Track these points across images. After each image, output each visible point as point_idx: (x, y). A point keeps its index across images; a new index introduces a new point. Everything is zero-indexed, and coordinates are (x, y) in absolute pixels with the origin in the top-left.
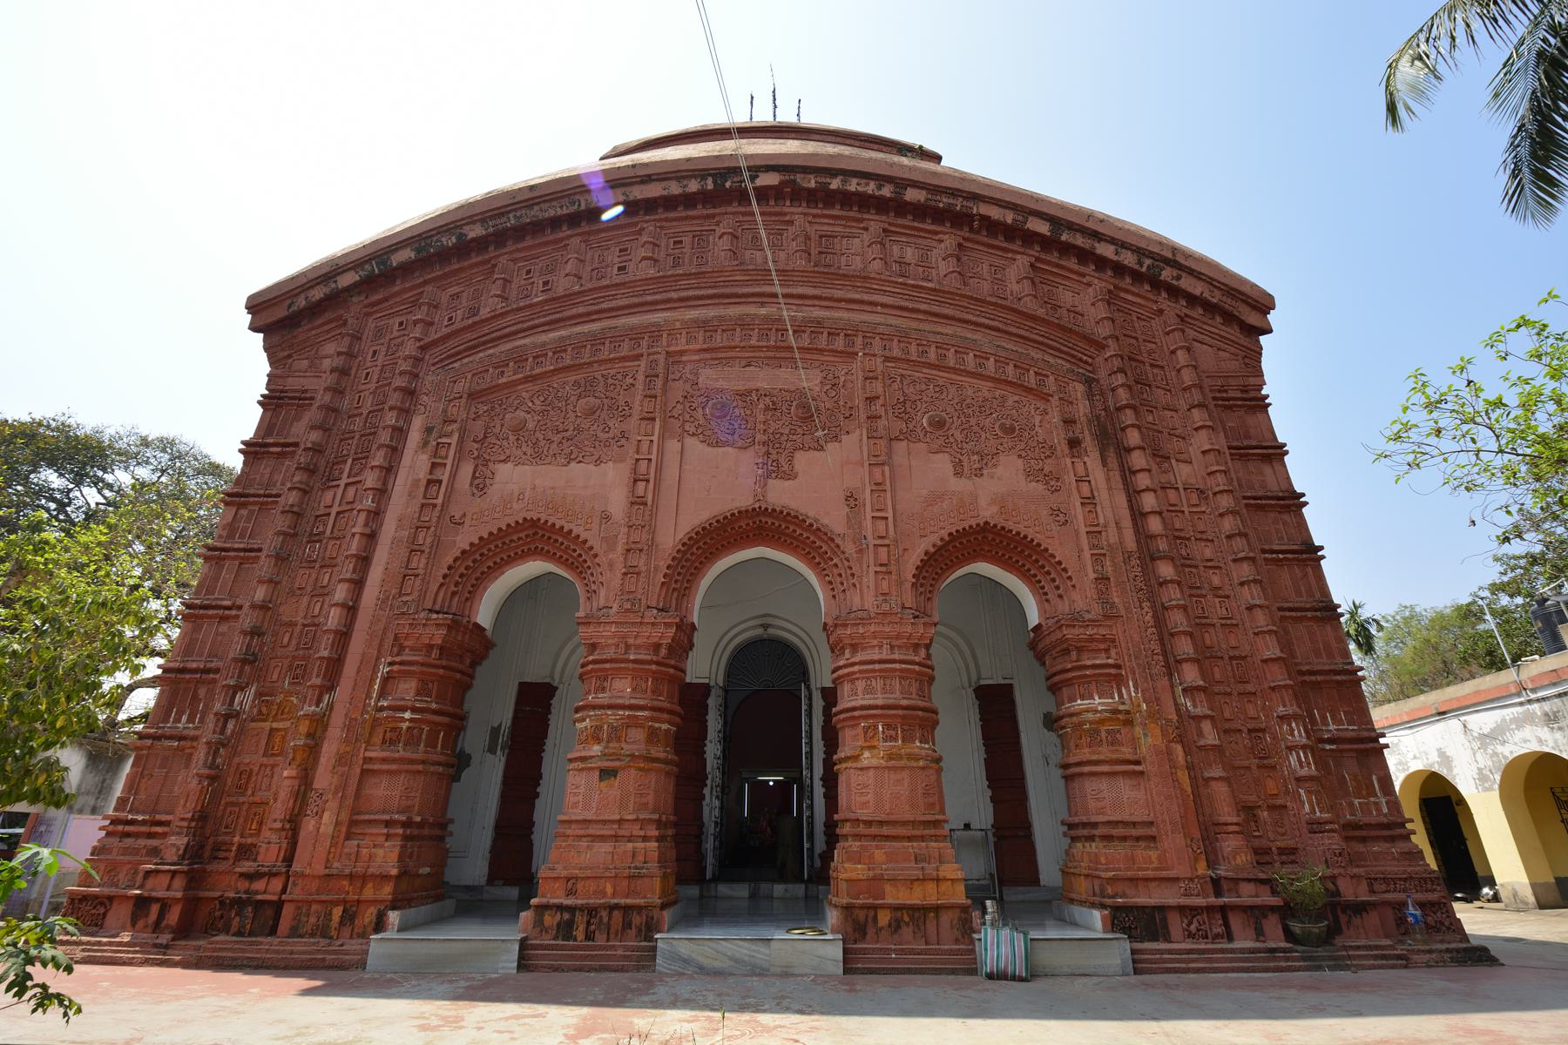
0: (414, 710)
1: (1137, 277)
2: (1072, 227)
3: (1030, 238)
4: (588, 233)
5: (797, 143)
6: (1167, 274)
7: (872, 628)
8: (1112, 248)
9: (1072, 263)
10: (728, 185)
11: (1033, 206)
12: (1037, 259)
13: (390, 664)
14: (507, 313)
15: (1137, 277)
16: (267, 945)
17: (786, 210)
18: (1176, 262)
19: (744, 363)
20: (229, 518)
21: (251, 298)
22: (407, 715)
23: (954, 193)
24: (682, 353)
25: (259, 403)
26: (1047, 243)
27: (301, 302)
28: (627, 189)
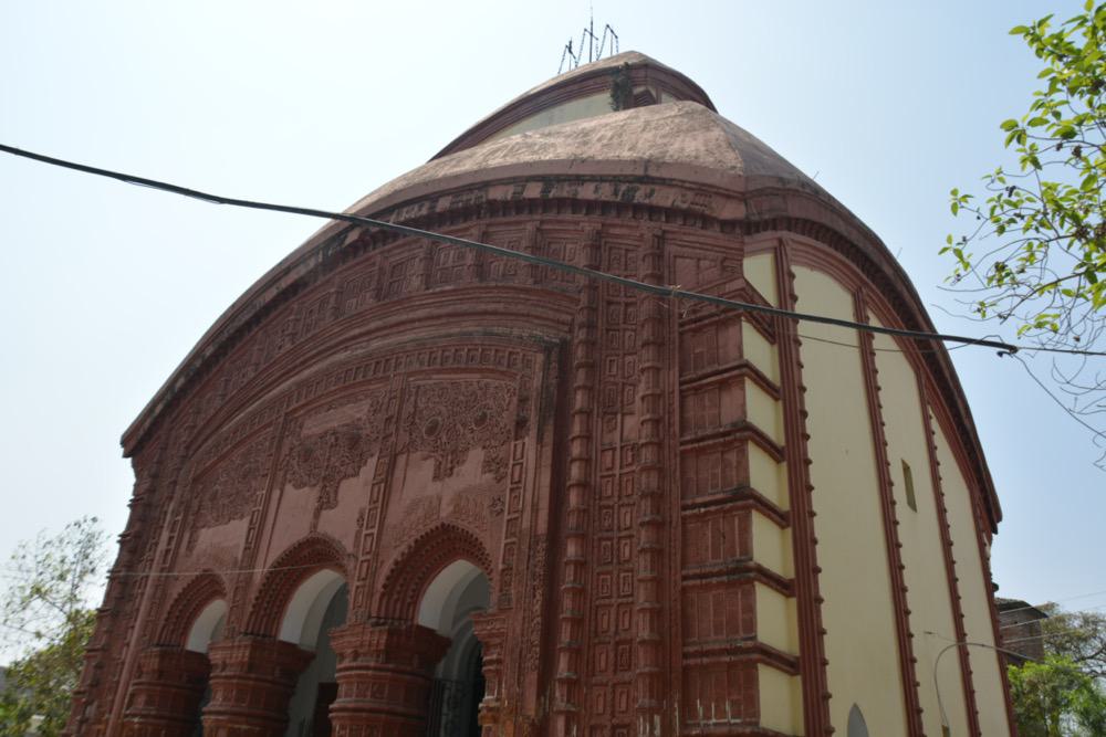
0: (143, 716)
1: (620, 208)
2: (560, 179)
3: (531, 205)
4: (266, 325)
5: (268, 300)
6: (639, 197)
7: (346, 639)
8: (592, 186)
9: (568, 216)
10: (330, 252)
11: (527, 173)
12: (542, 222)
13: (136, 684)
14: (196, 438)
15: (620, 208)
16: (784, 591)
17: (370, 254)
18: (647, 177)
19: (326, 407)
20: (613, 189)
21: (125, 441)
22: (136, 720)
23: (470, 188)
24: (295, 410)
25: (129, 506)
26: (544, 204)
27: (141, 432)
28: (278, 284)
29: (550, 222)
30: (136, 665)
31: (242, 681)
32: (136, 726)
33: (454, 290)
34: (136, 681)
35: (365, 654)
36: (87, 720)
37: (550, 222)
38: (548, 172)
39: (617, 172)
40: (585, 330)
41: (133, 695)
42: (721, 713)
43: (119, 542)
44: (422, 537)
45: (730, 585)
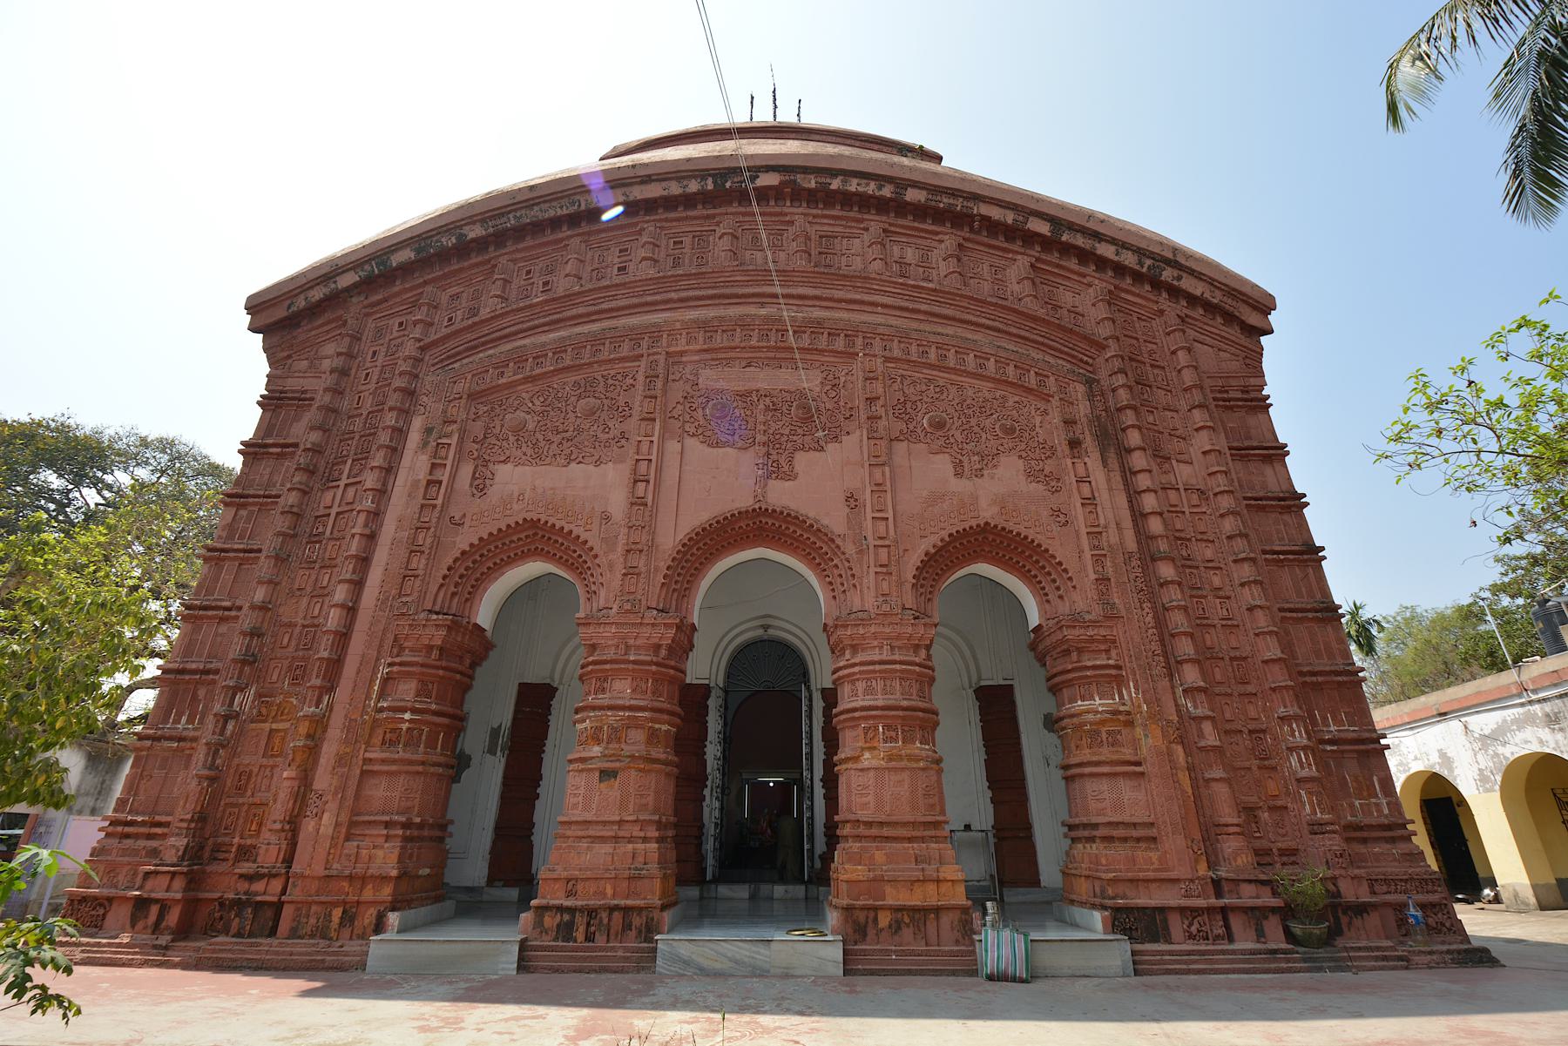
0: (414, 711)
2: (1072, 227)
3: (1030, 238)
10: (728, 185)
11: (1033, 206)
13: (390, 665)
15: (1138, 277)
17: (786, 210)
22: (407, 716)
23: (954, 193)
29: (1044, 262)
30: (390, 637)
31: (448, 674)
32: (405, 726)
33: (935, 290)
34: (389, 660)
35: (412, 650)
36: (237, 715)
37: (1044, 262)
38: (1060, 214)
39: (1143, 245)
40: (335, 376)
41: (387, 680)
42: (1337, 722)
43: (240, 452)
44: (1019, 534)
45: (1322, 620)
